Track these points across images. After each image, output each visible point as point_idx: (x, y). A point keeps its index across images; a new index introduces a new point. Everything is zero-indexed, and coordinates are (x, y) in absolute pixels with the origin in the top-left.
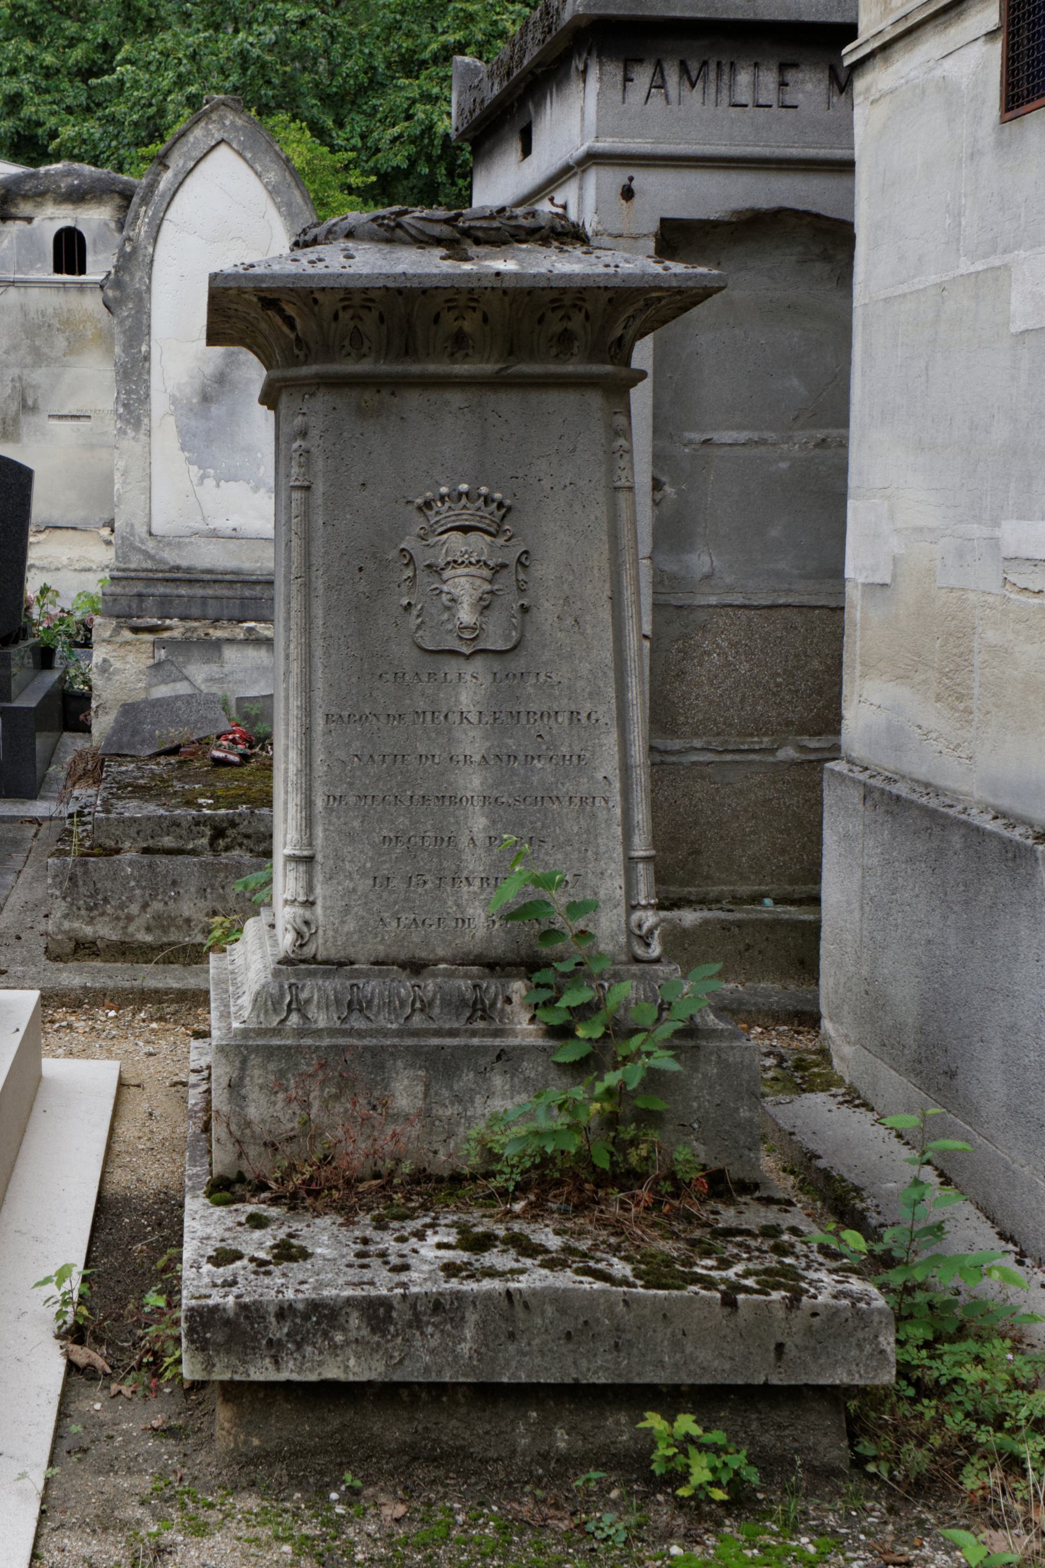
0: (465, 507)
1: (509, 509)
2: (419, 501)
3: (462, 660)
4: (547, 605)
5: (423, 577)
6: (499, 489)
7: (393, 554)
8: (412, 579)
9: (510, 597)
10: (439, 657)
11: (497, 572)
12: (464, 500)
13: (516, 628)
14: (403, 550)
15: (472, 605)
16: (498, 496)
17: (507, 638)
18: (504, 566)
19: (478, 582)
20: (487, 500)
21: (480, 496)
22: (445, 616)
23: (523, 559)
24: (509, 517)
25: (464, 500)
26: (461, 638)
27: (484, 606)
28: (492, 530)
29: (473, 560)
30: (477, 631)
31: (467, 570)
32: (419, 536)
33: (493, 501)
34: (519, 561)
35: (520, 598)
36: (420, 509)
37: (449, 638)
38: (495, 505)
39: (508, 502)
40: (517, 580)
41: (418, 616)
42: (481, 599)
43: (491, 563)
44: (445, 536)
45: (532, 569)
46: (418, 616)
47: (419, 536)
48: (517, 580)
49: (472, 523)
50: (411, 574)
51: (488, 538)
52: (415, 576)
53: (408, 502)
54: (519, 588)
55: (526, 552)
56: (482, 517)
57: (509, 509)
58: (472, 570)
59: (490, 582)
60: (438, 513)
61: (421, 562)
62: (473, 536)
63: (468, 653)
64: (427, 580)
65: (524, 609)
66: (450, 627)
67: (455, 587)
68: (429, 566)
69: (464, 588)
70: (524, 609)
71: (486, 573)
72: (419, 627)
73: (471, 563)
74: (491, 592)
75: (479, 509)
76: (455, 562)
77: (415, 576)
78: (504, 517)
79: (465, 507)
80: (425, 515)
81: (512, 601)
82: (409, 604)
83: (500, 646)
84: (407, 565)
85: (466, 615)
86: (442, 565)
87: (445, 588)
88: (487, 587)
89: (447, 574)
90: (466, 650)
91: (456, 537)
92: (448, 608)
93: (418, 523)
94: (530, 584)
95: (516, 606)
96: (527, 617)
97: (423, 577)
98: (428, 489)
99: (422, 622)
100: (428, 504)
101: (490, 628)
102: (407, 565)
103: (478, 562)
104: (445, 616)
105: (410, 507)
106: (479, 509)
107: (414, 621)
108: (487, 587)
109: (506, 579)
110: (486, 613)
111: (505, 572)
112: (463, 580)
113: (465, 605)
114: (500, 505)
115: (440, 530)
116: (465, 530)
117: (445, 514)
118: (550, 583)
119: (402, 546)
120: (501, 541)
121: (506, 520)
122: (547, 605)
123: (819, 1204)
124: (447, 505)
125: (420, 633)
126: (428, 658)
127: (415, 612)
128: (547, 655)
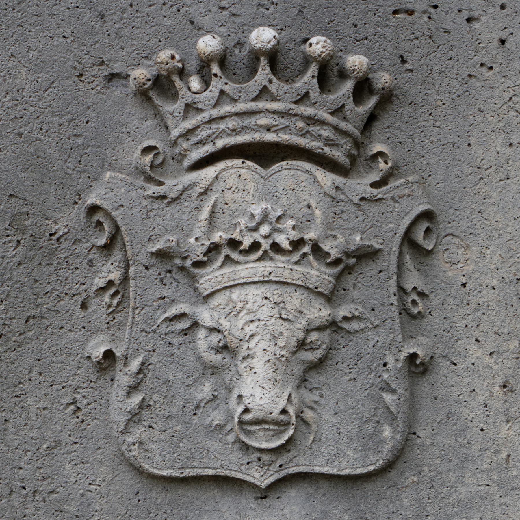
0: (264, 93)
1: (387, 98)
2: (141, 74)
3: (247, 501)
4: (476, 353)
5: (145, 285)
6: (360, 42)
7: (69, 219)
8: (118, 288)
9: (381, 337)
10: (190, 493)
11: (349, 270)
12: (263, 74)
13: (393, 419)
14: (94, 209)
15: (278, 363)
16: (356, 61)
17: (370, 442)
18: (366, 255)
19: (295, 300)
20: (328, 73)
21: (307, 61)
22: (206, 390)
23: (419, 236)
24: (387, 119)
25: (263, 74)
26: (246, 448)
27: (310, 362)
28: (337, 154)
29: (283, 240)
30: (293, 427)
31: (264, 268)
32: (140, 171)
33: (343, 75)
34: (408, 239)
35: (408, 336)
36: (143, 94)
37: (213, 445)
38: (348, 86)
39: (383, 79)
40: (401, 289)
41: (132, 389)
42: (302, 345)
43: (330, 247)
44: (210, 172)
45: (440, 260)
46: (132, 389)
47: (140, 171)
48: (401, 289)
49: (284, 137)
50: (115, 276)
51: (326, 178)
52: (125, 279)
53: (113, 77)
54: (404, 311)
55: (427, 215)
56: (311, 120)
57: (387, 98)
58: (279, 267)
59: (329, 298)
60: (190, 108)
61: (141, 245)
62: (287, 174)
63: (264, 483)
64: (156, 291)
65: (417, 367)
66: (216, 417)
67: (233, 313)
68: (163, 255)
69: (255, 314)
70: (417, 367)
71: (317, 274)
72: (134, 418)
73: (276, 247)
74: (333, 326)
75: (303, 98)
76: (234, 244)
77: (125, 279)
78: (372, 118)
79: (264, 93)
80: (158, 114)
81: (385, 345)
82: (109, 355)
83: (351, 463)
84: (108, 248)
85: (260, 389)
86: (198, 252)
87: (205, 316)
88: (319, 312)
89: (212, 277)
90: (260, 477)
91: (238, 172)
92: (214, 370)
93: (138, 134)
94: (435, 301)
95: (395, 361)
96: (424, 386)
97: (145, 285)
98: (168, 41)
99: (143, 405)
100: (162, 85)
101: (325, 419)
102: (108, 248)
103: (297, 244)
104: (206, 390)
105: (117, 91)
106: (303, 98)
107: (120, 403)
108: (319, 312)
109: (372, 292)
110: (315, 379)
111: (370, 270)
112: (254, 294)
113: (258, 364)
114: (363, 87)
115: (196, 155)
116: (264, 154)
117: (215, 110)
118: (488, 295)
119: (92, 199)
120: (360, 185)
121: (377, 128)
122: (476, 353)
123: (353, 248)
124: (216, 85)
125: (138, 432)
126: (159, 496)
127: (124, 378)
128: (470, 484)
